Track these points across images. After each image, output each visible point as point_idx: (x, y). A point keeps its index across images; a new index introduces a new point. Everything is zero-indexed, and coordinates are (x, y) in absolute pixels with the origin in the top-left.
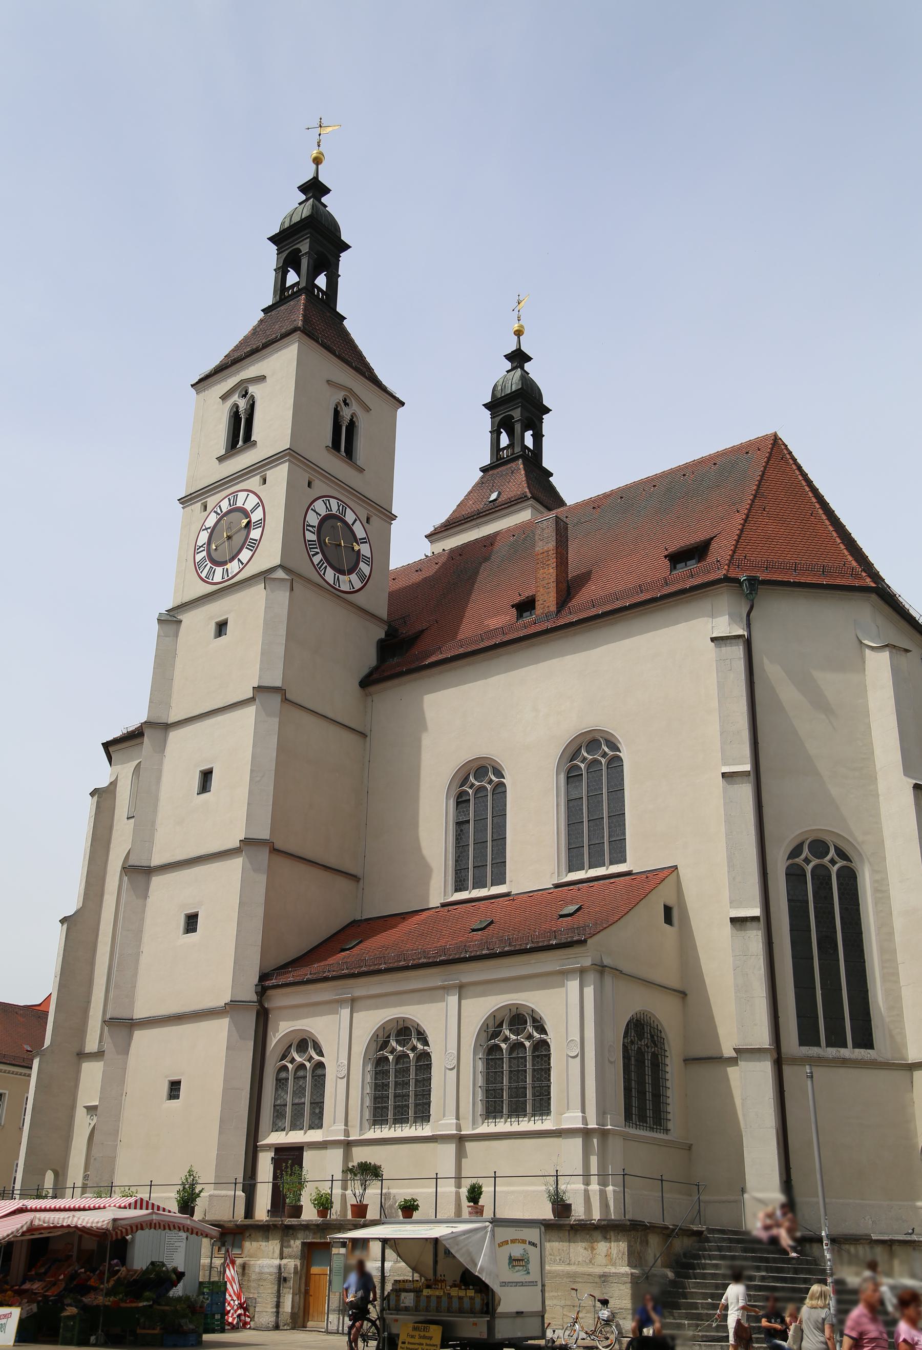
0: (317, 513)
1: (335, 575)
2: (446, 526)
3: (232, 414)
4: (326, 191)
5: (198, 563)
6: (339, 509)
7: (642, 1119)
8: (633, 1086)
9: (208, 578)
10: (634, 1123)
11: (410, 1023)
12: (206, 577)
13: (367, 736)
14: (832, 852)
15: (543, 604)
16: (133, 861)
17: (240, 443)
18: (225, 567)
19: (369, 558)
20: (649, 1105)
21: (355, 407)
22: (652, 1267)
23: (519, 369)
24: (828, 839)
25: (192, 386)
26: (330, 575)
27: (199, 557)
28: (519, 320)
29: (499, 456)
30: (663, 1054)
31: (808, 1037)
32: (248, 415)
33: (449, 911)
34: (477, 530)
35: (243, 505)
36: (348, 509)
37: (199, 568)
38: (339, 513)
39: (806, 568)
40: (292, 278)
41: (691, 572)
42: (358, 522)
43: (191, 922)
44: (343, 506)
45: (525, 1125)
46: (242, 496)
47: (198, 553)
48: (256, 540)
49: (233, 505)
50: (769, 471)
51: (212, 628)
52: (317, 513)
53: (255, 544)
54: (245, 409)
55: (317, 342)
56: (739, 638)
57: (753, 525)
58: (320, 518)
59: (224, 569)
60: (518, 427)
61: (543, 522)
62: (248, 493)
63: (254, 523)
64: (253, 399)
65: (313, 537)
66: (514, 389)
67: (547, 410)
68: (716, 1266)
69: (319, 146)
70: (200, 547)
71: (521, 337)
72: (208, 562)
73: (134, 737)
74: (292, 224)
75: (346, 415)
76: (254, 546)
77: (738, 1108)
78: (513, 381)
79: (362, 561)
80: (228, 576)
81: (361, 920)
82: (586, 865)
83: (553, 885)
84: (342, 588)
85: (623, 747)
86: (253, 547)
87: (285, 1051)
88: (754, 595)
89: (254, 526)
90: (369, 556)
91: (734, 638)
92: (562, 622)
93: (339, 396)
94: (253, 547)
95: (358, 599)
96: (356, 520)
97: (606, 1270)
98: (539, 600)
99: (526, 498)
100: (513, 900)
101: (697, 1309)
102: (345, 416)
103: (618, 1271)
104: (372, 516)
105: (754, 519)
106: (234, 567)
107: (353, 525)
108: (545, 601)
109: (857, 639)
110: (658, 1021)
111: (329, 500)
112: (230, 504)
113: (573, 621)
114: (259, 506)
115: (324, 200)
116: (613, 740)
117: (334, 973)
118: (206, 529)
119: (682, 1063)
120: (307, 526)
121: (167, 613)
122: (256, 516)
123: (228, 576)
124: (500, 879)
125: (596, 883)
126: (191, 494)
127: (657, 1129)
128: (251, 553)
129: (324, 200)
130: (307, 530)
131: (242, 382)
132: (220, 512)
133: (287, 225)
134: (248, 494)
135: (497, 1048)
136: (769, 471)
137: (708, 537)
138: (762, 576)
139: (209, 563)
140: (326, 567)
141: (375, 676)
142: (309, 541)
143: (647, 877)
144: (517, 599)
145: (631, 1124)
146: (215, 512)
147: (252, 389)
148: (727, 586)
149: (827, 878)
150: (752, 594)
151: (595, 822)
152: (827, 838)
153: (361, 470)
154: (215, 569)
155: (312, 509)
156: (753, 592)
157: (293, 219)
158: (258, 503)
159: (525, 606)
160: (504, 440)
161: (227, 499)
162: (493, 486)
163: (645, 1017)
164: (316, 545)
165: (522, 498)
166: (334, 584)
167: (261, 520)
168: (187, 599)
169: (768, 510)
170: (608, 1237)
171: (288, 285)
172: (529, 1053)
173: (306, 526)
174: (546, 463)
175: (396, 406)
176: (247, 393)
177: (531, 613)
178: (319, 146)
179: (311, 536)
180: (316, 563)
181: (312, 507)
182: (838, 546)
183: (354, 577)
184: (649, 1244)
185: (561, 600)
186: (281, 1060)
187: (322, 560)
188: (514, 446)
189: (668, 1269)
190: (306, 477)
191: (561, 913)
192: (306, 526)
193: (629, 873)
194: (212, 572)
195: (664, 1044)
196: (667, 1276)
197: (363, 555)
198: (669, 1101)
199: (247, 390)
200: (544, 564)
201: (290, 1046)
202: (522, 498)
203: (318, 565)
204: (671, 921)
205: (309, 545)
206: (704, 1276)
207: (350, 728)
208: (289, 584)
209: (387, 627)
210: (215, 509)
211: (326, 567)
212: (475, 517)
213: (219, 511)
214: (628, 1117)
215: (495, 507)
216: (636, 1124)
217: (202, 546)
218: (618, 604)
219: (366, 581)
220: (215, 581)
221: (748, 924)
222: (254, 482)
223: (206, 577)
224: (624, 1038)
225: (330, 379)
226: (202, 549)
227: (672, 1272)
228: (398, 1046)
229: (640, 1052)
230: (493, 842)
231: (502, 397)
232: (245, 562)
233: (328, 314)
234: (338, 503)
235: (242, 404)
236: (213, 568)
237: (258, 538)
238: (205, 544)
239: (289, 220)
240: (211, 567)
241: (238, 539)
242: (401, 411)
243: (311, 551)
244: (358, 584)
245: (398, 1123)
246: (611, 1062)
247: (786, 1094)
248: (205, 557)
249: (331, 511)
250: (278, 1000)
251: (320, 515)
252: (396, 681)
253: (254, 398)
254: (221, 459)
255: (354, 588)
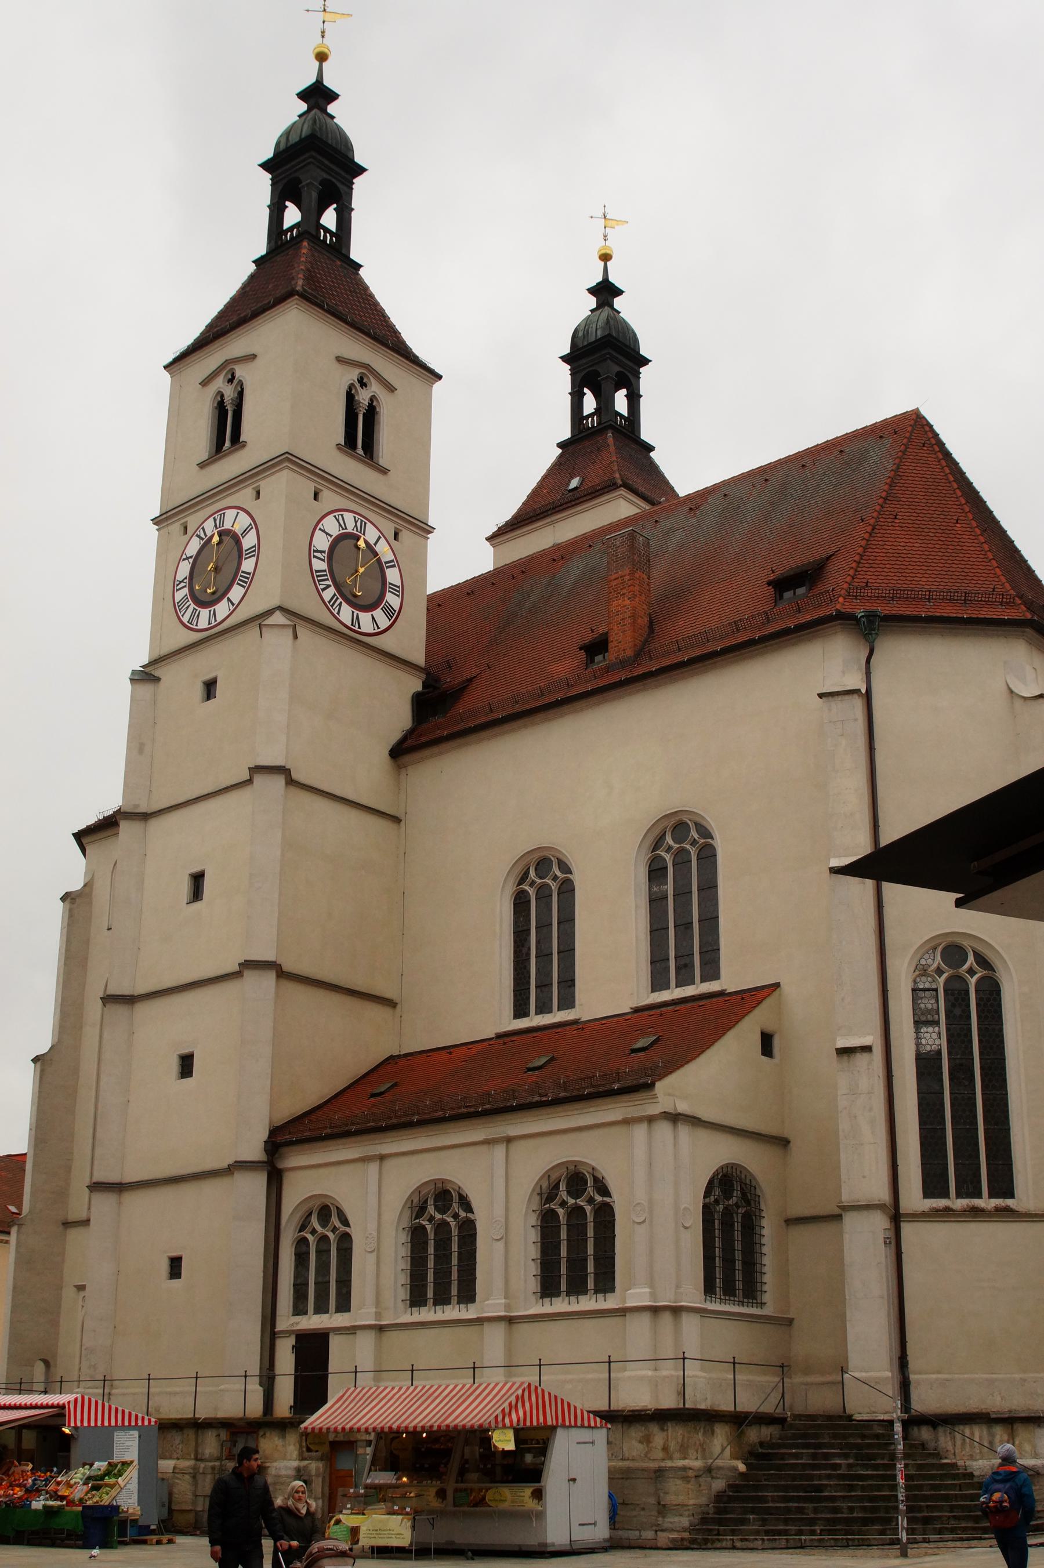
0: (327, 534)
1: (353, 612)
2: (511, 525)
3: (216, 405)
4: (332, 96)
5: (178, 603)
6: (356, 526)
7: (729, 1291)
8: (717, 1255)
9: (191, 624)
10: (759, 1301)
11: (450, 1185)
12: (188, 622)
13: (401, 820)
14: (971, 958)
15: (618, 646)
16: (110, 992)
17: (227, 444)
18: (212, 609)
19: (398, 587)
20: (738, 1276)
21: (375, 387)
22: (716, 1458)
23: (606, 308)
24: (965, 943)
25: (165, 367)
26: (346, 613)
27: (179, 596)
28: (605, 240)
29: (582, 426)
30: (758, 1214)
31: (934, 1185)
32: (236, 406)
33: (505, 1044)
34: (550, 529)
35: (232, 526)
36: (369, 524)
37: (180, 610)
38: (357, 531)
39: (943, 596)
40: (292, 215)
41: (798, 605)
42: (382, 540)
43: (186, 1065)
44: (362, 521)
45: (587, 1303)
46: (230, 514)
47: (177, 590)
48: (249, 574)
49: (220, 527)
50: (906, 464)
51: (199, 690)
52: (327, 534)
53: (248, 578)
54: (232, 399)
55: (322, 307)
56: (853, 693)
57: (880, 539)
58: (331, 540)
59: (210, 611)
60: (606, 386)
61: (616, 537)
62: (239, 511)
63: (246, 551)
64: (242, 385)
65: (323, 566)
66: (599, 336)
67: (645, 362)
68: (796, 1456)
69: (323, 37)
70: (181, 582)
71: (608, 263)
72: (191, 602)
73: (107, 825)
74: (289, 145)
75: (363, 399)
76: (248, 581)
77: (24, 1202)
78: (598, 324)
79: (389, 591)
80: (216, 621)
81: (400, 1055)
82: (673, 983)
83: (631, 1008)
84: (363, 630)
85: (716, 834)
86: (246, 583)
87: (305, 1220)
88: (874, 636)
89: (246, 555)
90: (399, 584)
91: (847, 694)
92: (640, 671)
93: (353, 375)
94: (246, 583)
95: (385, 642)
96: (379, 538)
97: (663, 1464)
98: (612, 641)
99: (614, 487)
100: (583, 1029)
101: (767, 1502)
102: (362, 401)
103: (674, 1465)
104: (401, 530)
105: (881, 531)
106: (222, 609)
107: (375, 544)
108: (620, 642)
109: (1006, 687)
110: (751, 1175)
111: (342, 515)
112: (216, 525)
113: (652, 671)
114: (252, 528)
115: (331, 109)
116: (704, 823)
117: (358, 1126)
118: (187, 558)
119: (783, 1224)
120: (314, 551)
121: (141, 669)
122: (249, 541)
123: (216, 621)
124: (567, 1001)
125: (683, 1006)
126: (167, 512)
127: (748, 1303)
128: (243, 590)
129: (331, 109)
130: (315, 557)
131: (227, 362)
132: (204, 537)
133: (282, 146)
134: (238, 513)
135: (553, 1212)
136: (906, 464)
137: (824, 556)
138: (882, 609)
139: (192, 604)
140: (341, 603)
141: (410, 742)
142: (317, 571)
143: (743, 998)
144: (588, 638)
145: (713, 1299)
146: (197, 536)
147: (240, 372)
148: (841, 624)
149: (963, 992)
150: (871, 634)
151: (684, 927)
152: (964, 943)
153: (384, 471)
154: (200, 611)
155: (320, 529)
156: (873, 632)
157: (290, 138)
158: (251, 524)
159: (597, 647)
160: (590, 403)
161: (211, 519)
162: (574, 468)
163: (734, 1170)
164: (326, 575)
165: (610, 486)
166: (352, 625)
167: (255, 546)
168: (165, 651)
169: (901, 517)
170: (665, 1428)
171: (286, 226)
172: (590, 1218)
173: (312, 552)
174: (646, 435)
175: (431, 381)
176: (233, 377)
177: (604, 657)
178: (323, 37)
179: (320, 565)
180: (327, 598)
181: (320, 526)
182: (989, 564)
183: (378, 613)
184: (715, 1435)
185: (639, 640)
186: (300, 1231)
187: (335, 595)
188: (601, 413)
189: (740, 1461)
190: (309, 487)
191: (531, 1065)
192: (312, 552)
193: (721, 994)
194: (196, 616)
195: (759, 1203)
196: (736, 1469)
197: (390, 584)
198: (765, 1269)
199: (233, 373)
200: (619, 593)
201: (310, 1214)
202: (610, 486)
203: (329, 602)
204: (772, 1053)
205: (318, 576)
206: (779, 1468)
207: (378, 811)
208: (290, 631)
209: (424, 676)
210: (198, 532)
211: (341, 603)
212: (549, 513)
213: (202, 535)
214: (709, 1289)
215: (575, 499)
216: (721, 1299)
217: (182, 581)
218: (711, 648)
219: (394, 614)
220: (200, 627)
221: (858, 1055)
222: (244, 496)
223: (188, 622)
224: (705, 1197)
225: (339, 355)
226: (183, 584)
227: (744, 1463)
228: (436, 1213)
229: (728, 1213)
230: (560, 954)
231: (584, 347)
232: (236, 602)
233: (339, 263)
234: (355, 517)
235: (229, 392)
236: (197, 610)
237: (251, 570)
238: (186, 578)
239: (285, 138)
240: (194, 609)
241: (228, 572)
242: (438, 386)
243: (320, 585)
244: (384, 622)
245: (440, 1305)
246: (686, 1228)
247: (903, 1256)
248: (186, 595)
249: (346, 529)
250: (294, 1159)
251: (331, 536)
252: (435, 749)
253: (242, 384)
254: (202, 465)
255: (378, 628)
